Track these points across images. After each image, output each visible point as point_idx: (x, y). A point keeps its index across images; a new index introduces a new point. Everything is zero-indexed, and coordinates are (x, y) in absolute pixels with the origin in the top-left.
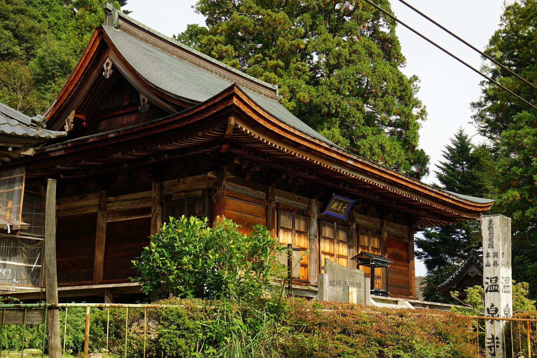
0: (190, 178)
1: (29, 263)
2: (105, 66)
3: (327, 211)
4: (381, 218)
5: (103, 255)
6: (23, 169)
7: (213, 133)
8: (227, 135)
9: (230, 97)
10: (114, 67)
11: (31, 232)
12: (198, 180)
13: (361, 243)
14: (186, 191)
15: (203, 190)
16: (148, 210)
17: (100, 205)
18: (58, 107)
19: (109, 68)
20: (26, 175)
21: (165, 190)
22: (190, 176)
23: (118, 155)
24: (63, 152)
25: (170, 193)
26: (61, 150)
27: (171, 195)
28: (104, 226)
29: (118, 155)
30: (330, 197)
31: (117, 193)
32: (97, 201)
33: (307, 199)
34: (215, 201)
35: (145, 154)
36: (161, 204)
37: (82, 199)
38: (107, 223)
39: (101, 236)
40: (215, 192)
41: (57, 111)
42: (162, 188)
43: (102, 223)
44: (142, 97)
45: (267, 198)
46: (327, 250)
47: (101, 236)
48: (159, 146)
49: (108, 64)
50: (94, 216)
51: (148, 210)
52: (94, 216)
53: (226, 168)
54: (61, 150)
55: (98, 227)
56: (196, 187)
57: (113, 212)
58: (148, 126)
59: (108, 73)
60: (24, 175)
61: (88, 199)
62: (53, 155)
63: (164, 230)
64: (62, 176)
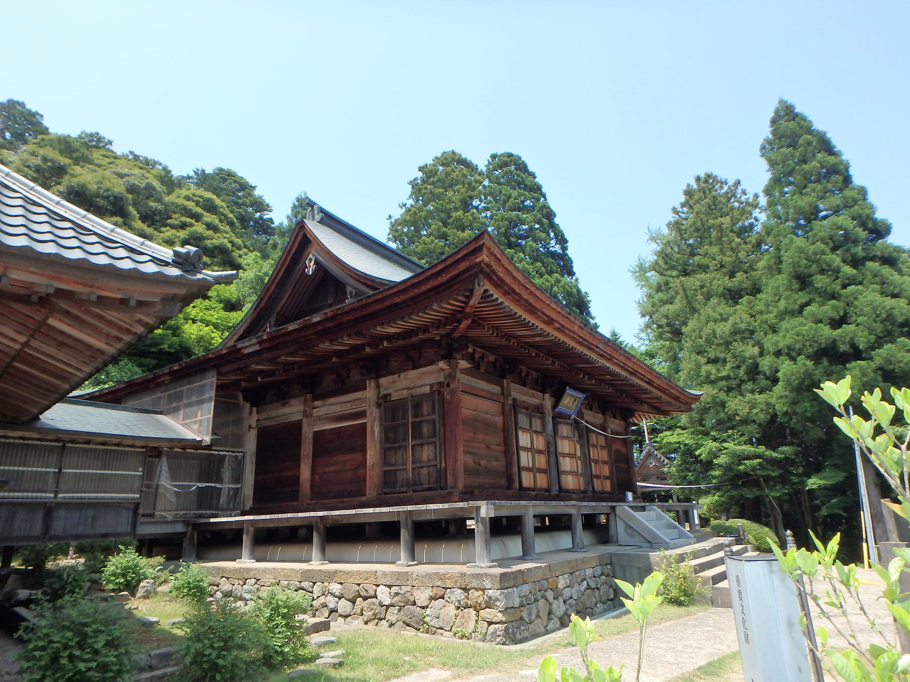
0: (415, 371)
1: (234, 483)
2: (307, 262)
3: (560, 408)
4: (603, 413)
5: (310, 470)
6: (214, 373)
7: (450, 305)
8: (471, 307)
9: (479, 249)
10: (317, 262)
11: (226, 446)
12: (424, 374)
13: (591, 442)
14: (409, 389)
15: (431, 386)
16: (362, 414)
17: (305, 412)
18: (258, 310)
19: (313, 263)
20: (218, 379)
21: (381, 389)
22: (413, 369)
23: (325, 346)
24: (257, 348)
25: (388, 392)
26: (255, 344)
27: (390, 395)
28: (311, 436)
29: (325, 346)
30: (564, 390)
31: (324, 396)
32: (301, 408)
33: (540, 394)
34: (447, 397)
35: (359, 342)
36: (379, 405)
37: (284, 405)
38: (315, 432)
39: (307, 448)
40: (448, 385)
41: (258, 315)
42: (378, 386)
43: (308, 432)
44: (348, 289)
45: (503, 394)
46: (566, 451)
47: (307, 448)
48: (378, 328)
49: (310, 260)
50: (298, 425)
51: (362, 414)
52: (298, 425)
53: (458, 356)
54: (255, 344)
55: (303, 437)
56: (421, 382)
57: (320, 418)
58: (364, 302)
59: (311, 269)
60: (214, 379)
61: (291, 406)
62: (246, 351)
63: (643, 349)
64: (259, 379)
